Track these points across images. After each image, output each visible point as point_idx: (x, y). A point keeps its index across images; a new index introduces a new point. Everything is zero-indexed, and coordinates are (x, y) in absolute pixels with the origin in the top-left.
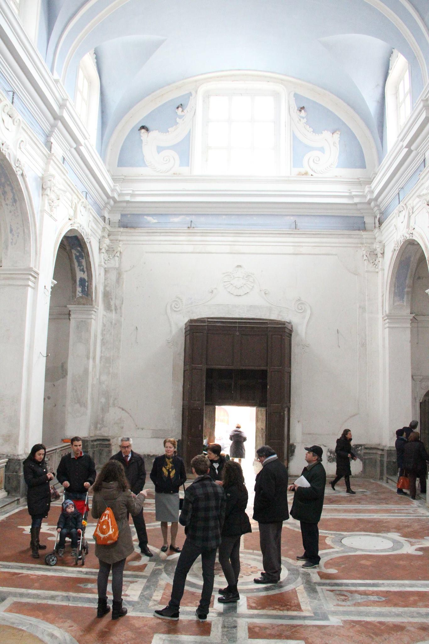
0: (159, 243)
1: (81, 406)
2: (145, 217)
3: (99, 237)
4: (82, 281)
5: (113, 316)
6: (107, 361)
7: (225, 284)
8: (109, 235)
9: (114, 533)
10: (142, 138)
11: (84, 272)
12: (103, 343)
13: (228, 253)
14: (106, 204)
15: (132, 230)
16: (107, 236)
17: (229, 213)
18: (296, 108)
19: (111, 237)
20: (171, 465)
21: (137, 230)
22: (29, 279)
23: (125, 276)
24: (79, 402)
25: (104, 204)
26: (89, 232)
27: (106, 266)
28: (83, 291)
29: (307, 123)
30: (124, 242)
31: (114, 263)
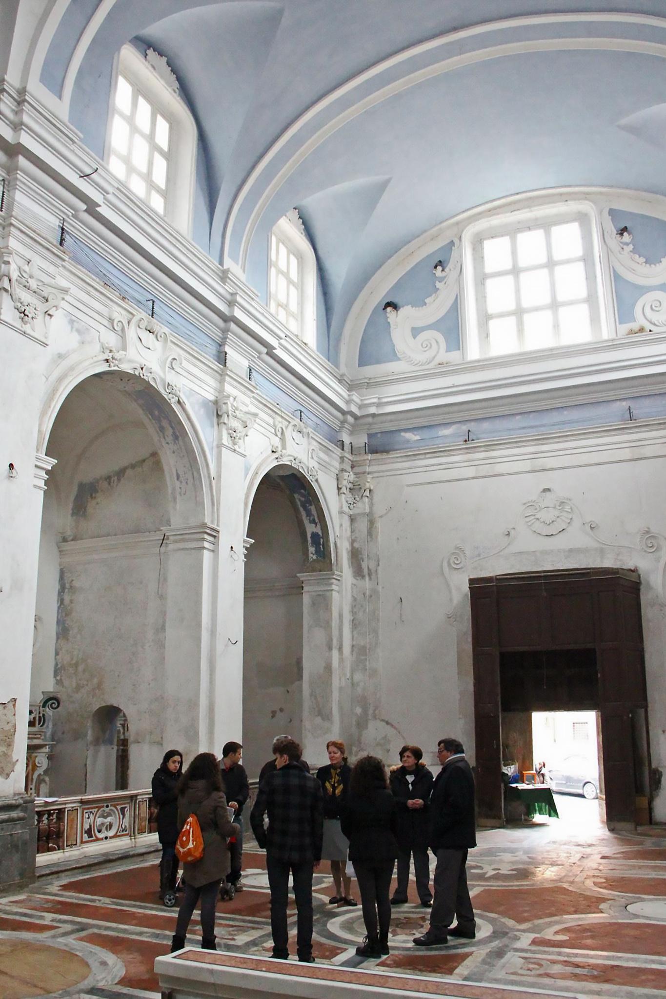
0: (425, 469)
1: (323, 719)
2: (403, 434)
3: (337, 472)
4: (315, 536)
5: (367, 584)
6: (361, 652)
7: (527, 519)
8: (352, 467)
9: (195, 847)
10: (389, 320)
11: (316, 524)
12: (355, 624)
13: (529, 472)
14: (343, 422)
15: (385, 456)
16: (349, 469)
17: (506, 413)
18: (615, 232)
19: (356, 470)
20: (337, 778)
21: (393, 455)
22: (204, 539)
23: (379, 524)
24: (320, 713)
25: (338, 423)
26: (313, 464)
27: (351, 513)
28: (317, 552)
29: (634, 251)
30: (376, 475)
31: (363, 506)
